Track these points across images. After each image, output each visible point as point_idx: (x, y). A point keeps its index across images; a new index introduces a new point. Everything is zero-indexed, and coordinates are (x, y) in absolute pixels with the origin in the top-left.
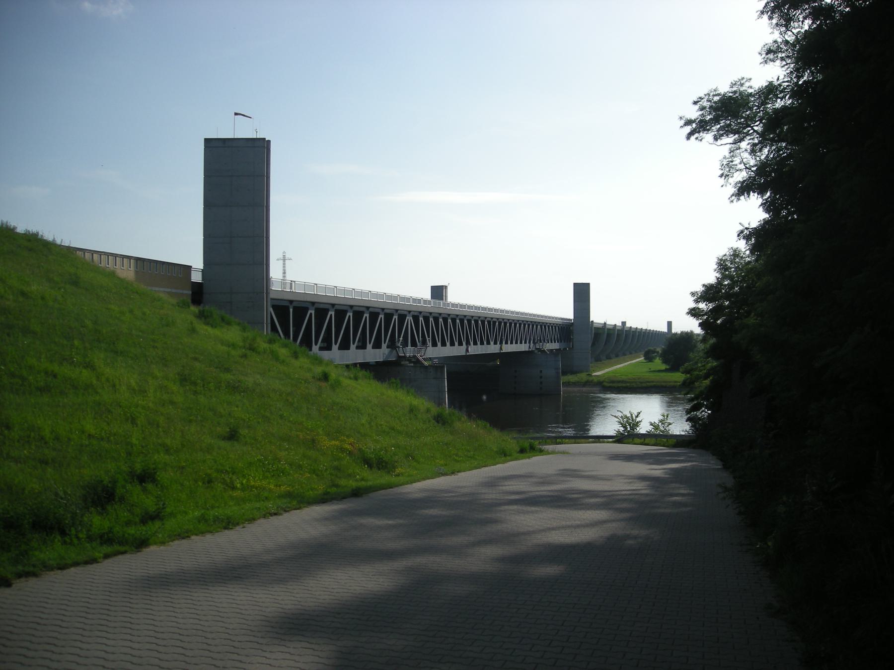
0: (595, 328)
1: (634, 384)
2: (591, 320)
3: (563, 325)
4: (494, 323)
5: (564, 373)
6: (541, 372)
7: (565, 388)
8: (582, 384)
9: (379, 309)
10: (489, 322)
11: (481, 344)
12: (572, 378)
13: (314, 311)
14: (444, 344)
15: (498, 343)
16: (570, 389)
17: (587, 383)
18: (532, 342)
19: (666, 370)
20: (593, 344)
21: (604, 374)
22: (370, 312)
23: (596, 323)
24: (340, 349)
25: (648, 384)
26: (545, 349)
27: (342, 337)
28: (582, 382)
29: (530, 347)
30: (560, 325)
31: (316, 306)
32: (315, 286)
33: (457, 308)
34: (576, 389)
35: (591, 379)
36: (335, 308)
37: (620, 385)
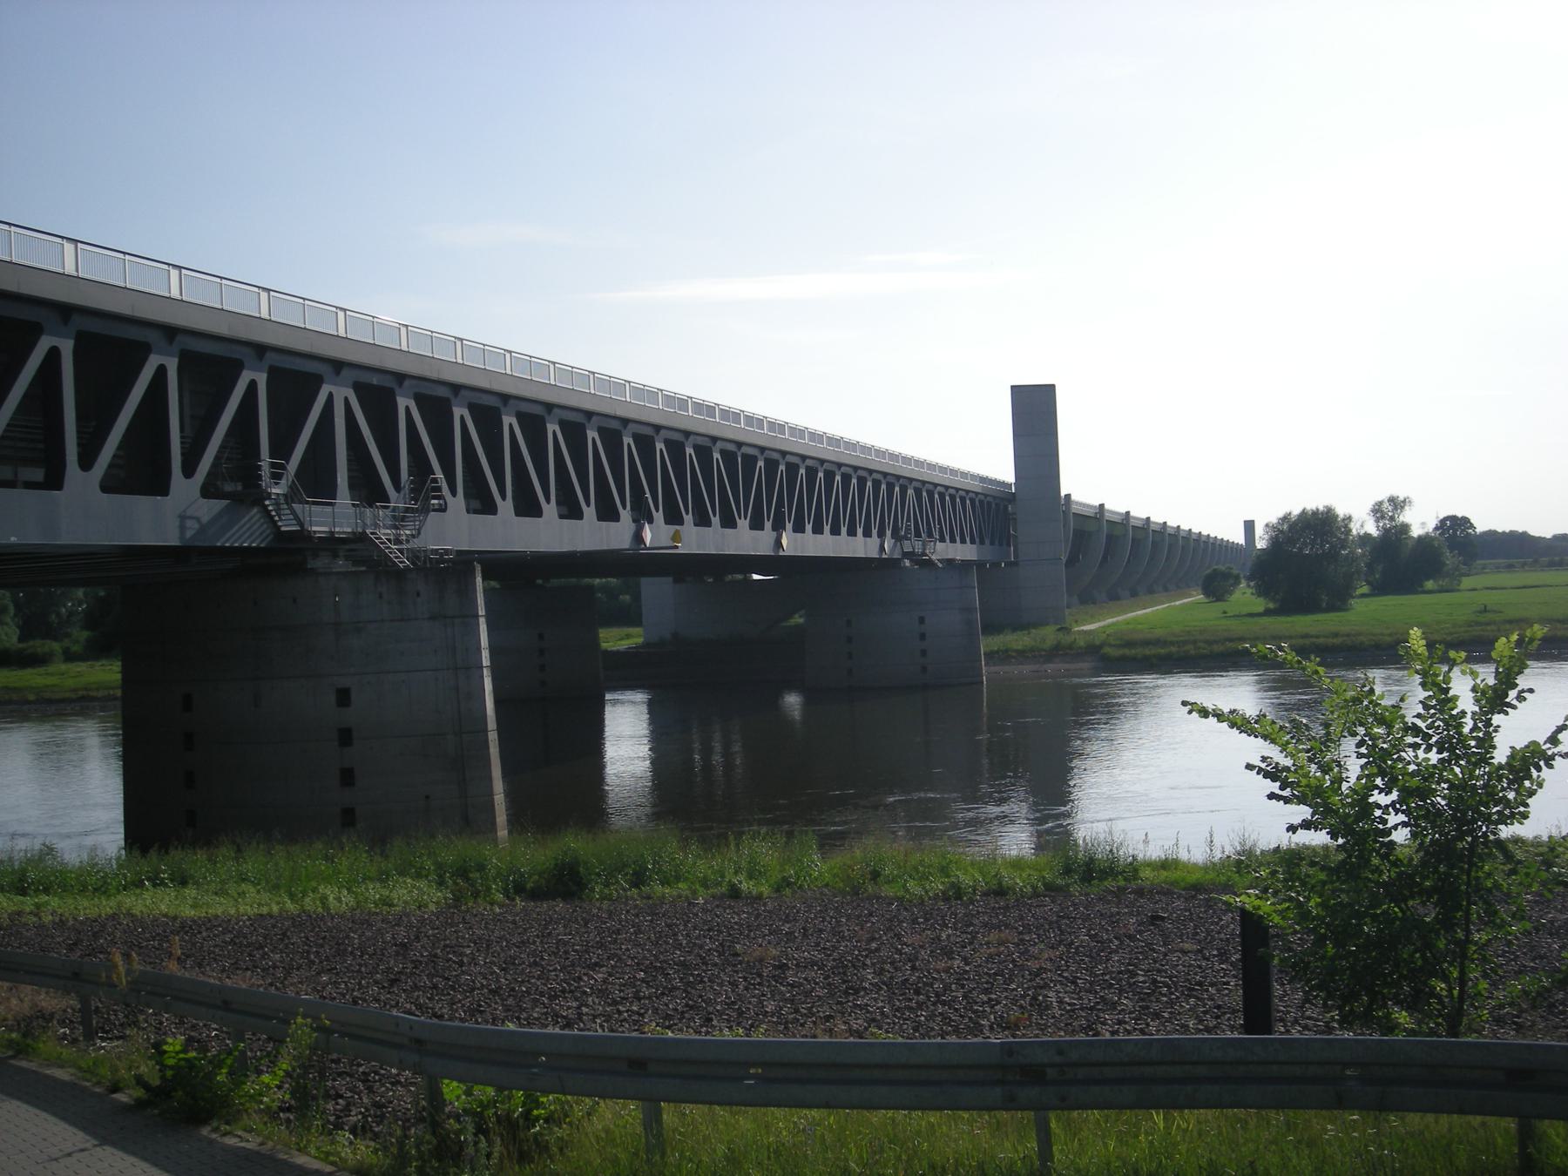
0: (1074, 513)
1: (1189, 647)
2: (1063, 494)
3: (986, 496)
4: (750, 461)
5: (990, 628)
6: (922, 620)
7: (993, 669)
8: (1043, 653)
9: (815, 461)
10: (728, 457)
11: (971, 543)
12: (1017, 640)
13: (631, 439)
14: (818, 530)
15: (875, 532)
16: (1014, 670)
17: (1057, 652)
18: (889, 533)
19: (1268, 612)
20: (1072, 561)
21: (1104, 627)
22: (825, 470)
23: (1077, 503)
24: (109, 485)
25: (1229, 644)
26: (933, 557)
27: (692, 503)
28: (1045, 650)
29: (882, 548)
30: (977, 494)
31: (271, 358)
32: (459, 343)
33: (885, 459)
34: (1027, 669)
35: (1066, 639)
36: (765, 455)
37: (1147, 651)
